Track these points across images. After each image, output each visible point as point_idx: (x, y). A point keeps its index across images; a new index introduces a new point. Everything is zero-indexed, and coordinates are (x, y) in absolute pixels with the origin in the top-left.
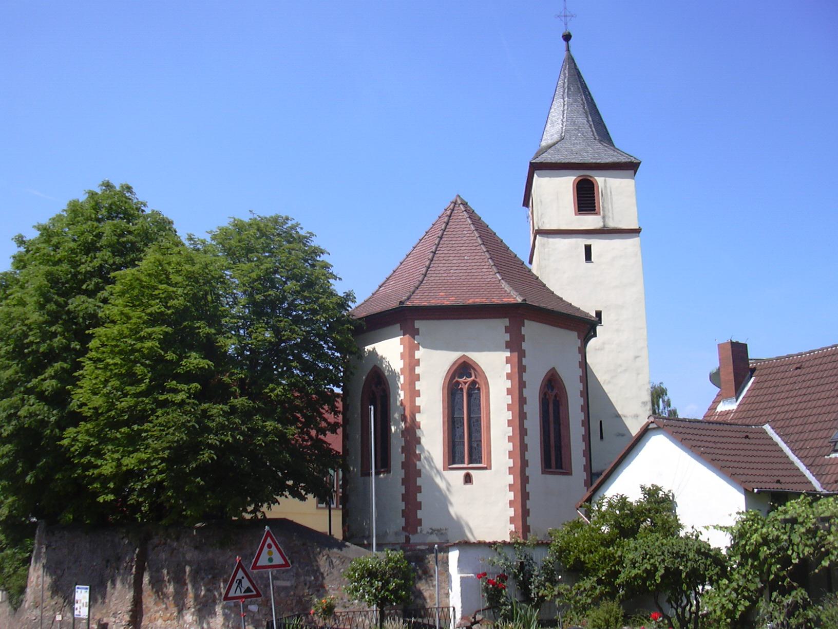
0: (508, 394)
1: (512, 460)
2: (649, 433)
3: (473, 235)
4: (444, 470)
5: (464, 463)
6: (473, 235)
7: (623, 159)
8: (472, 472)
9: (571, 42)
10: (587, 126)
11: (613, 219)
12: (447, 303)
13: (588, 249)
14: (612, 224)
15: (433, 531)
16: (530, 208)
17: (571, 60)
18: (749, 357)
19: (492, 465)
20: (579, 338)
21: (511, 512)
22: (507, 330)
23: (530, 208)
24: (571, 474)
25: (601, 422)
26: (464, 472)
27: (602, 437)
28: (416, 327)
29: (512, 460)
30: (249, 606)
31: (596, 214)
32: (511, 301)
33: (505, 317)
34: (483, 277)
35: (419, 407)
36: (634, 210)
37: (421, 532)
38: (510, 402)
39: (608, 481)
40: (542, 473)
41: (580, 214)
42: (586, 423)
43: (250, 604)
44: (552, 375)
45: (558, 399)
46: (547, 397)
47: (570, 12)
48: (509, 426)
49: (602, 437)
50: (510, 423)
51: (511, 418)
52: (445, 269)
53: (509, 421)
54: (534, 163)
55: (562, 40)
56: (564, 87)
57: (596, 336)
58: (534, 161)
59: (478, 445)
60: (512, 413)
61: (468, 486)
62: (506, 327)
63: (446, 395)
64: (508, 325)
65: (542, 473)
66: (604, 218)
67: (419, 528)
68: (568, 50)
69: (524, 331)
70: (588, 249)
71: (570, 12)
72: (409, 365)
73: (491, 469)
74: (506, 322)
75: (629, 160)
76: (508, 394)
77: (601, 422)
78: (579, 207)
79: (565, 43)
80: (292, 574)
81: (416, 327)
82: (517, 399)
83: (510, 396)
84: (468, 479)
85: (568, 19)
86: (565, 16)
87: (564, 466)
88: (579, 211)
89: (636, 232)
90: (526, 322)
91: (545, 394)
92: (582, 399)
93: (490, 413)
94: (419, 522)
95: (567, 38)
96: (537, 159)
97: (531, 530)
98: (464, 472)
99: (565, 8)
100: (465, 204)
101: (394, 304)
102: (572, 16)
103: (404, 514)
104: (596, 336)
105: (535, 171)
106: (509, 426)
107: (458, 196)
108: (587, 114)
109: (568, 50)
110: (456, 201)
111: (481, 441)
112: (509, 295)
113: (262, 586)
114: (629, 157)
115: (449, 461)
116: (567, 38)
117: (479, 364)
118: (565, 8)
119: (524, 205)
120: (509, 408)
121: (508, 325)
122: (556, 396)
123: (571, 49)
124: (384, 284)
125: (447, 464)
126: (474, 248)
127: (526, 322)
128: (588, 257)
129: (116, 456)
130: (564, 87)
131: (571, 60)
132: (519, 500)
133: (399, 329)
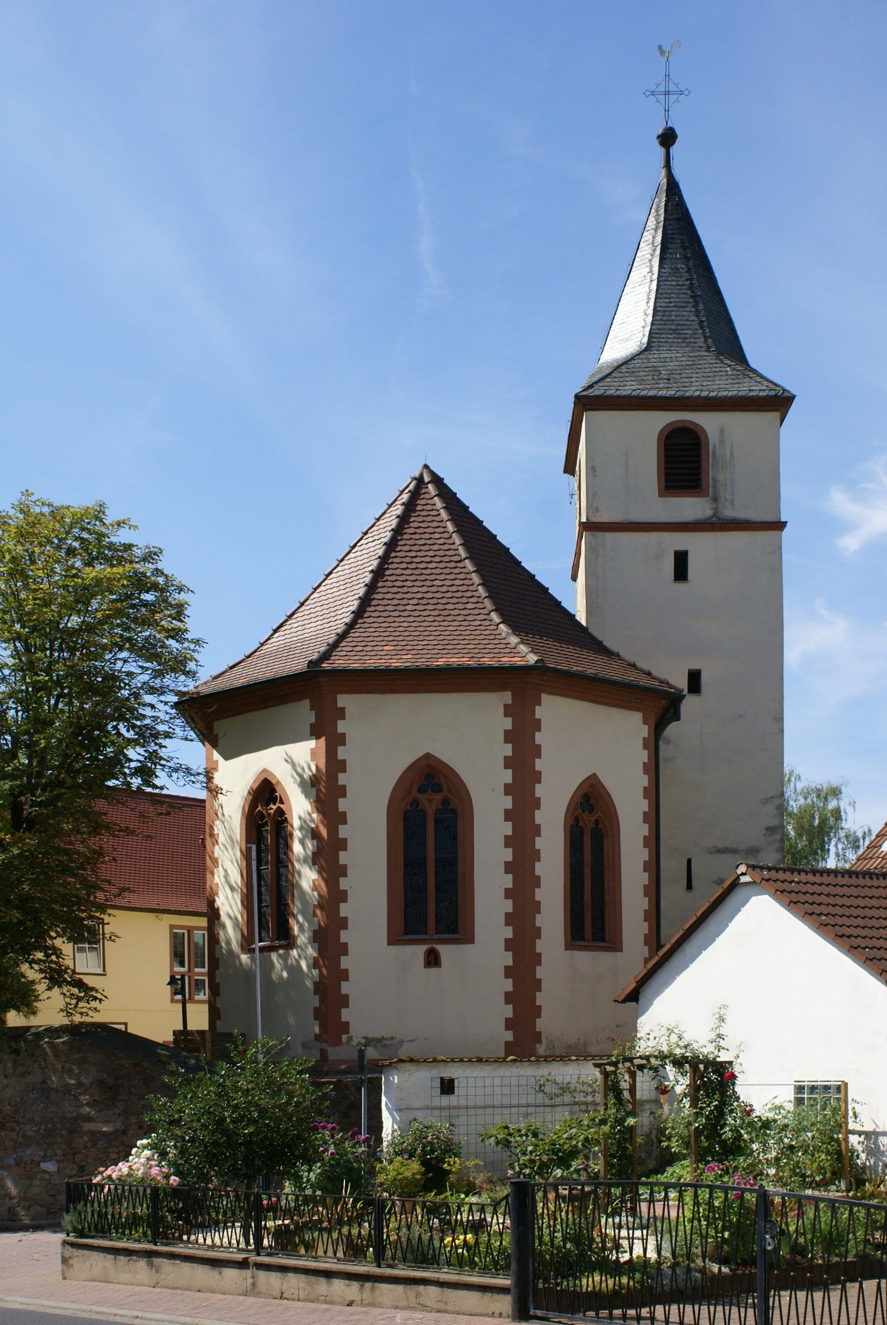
2: (738, 894)
3: (450, 541)
6: (450, 541)
7: (758, 390)
9: (674, 150)
11: (732, 503)
12: (395, 664)
13: (681, 561)
14: (729, 513)
15: (369, 1041)
16: (577, 477)
17: (673, 189)
20: (645, 723)
22: (508, 711)
23: (577, 477)
24: (621, 950)
25: (689, 861)
26: (424, 948)
27: (689, 886)
28: (340, 705)
30: (42, 1164)
32: (517, 661)
33: (504, 690)
34: (467, 618)
35: (506, 715)
37: (347, 1043)
39: (667, 963)
40: (567, 949)
42: (654, 866)
43: (44, 1161)
44: (591, 786)
45: (600, 826)
46: (581, 823)
47: (676, 85)
49: (689, 886)
52: (395, 602)
54: (587, 397)
55: (656, 143)
57: (678, 719)
58: (585, 393)
62: (506, 706)
64: (510, 702)
65: (567, 949)
67: (344, 1038)
68: (668, 165)
69: (540, 712)
70: (681, 561)
71: (676, 85)
74: (507, 697)
75: (772, 393)
77: (689, 861)
78: (667, 481)
79: (662, 150)
80: (117, 1112)
81: (340, 705)
85: (672, 98)
87: (607, 937)
90: (545, 697)
91: (577, 819)
92: (646, 827)
94: (345, 1027)
95: (668, 138)
96: (591, 391)
97: (543, 1039)
98: (424, 948)
99: (668, 76)
100: (437, 481)
103: (318, 1014)
104: (678, 719)
107: (426, 467)
109: (668, 165)
110: (421, 476)
112: (513, 651)
113: (64, 1132)
114: (773, 387)
116: (668, 138)
117: (455, 769)
118: (668, 76)
119: (566, 471)
122: (597, 822)
123: (674, 164)
124: (281, 626)
126: (452, 565)
127: (545, 697)
128: (681, 571)
130: (653, 243)
131: (673, 189)
133: (309, 708)
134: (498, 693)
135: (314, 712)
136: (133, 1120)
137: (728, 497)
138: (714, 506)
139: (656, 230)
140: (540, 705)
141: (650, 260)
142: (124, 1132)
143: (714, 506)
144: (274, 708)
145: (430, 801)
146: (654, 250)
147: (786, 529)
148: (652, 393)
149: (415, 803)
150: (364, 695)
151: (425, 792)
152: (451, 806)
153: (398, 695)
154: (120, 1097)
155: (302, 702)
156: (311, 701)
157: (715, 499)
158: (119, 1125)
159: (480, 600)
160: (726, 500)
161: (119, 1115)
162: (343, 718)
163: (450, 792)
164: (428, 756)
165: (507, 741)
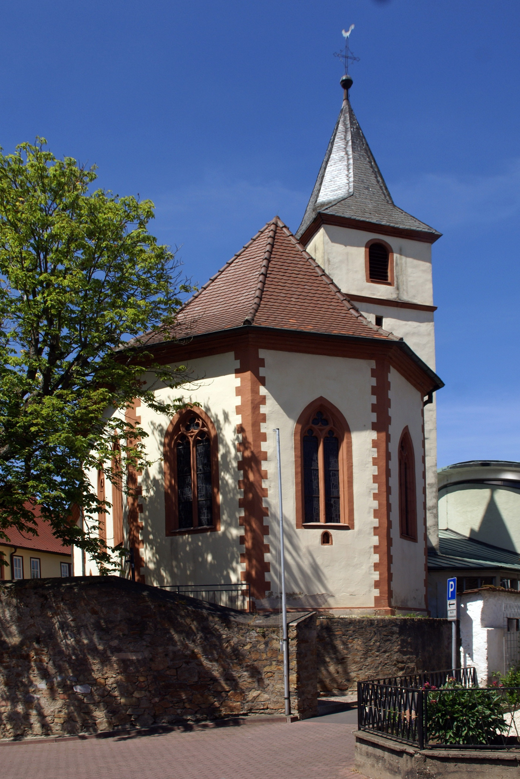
0: (373, 447)
1: (377, 520)
4: (298, 526)
5: (319, 521)
6: (308, 263)
7: (422, 228)
8: (331, 531)
9: (351, 90)
10: (378, 187)
11: (407, 293)
14: (406, 298)
18: (81, 575)
19: (355, 524)
21: (376, 576)
22: (374, 373)
26: (321, 531)
29: (377, 520)
31: (389, 284)
33: (371, 359)
36: (429, 287)
38: (376, 456)
41: (372, 282)
47: (352, 53)
48: (374, 482)
50: (375, 479)
51: (376, 473)
53: (374, 476)
56: (345, 139)
59: (335, 502)
60: (378, 468)
61: (326, 546)
62: (372, 370)
63: (299, 442)
66: (398, 289)
71: (352, 53)
72: (252, 403)
73: (353, 528)
74: (373, 364)
76: (373, 447)
78: (370, 274)
79: (343, 92)
82: (384, 454)
83: (375, 449)
84: (326, 539)
86: (347, 57)
88: (371, 278)
89: (431, 309)
93: (352, 466)
98: (321, 531)
101: (239, 323)
102: (355, 59)
105: (323, 225)
106: (374, 482)
108: (375, 174)
111: (339, 498)
115: (303, 520)
120: (375, 462)
121: (375, 367)
125: (301, 520)
129: (22, 420)
132: (386, 563)
134: (367, 361)
135: (239, 361)
136: (160, 649)
137: (405, 288)
138: (397, 292)
139: (346, 132)
140: (390, 372)
141: (345, 148)
142: (152, 660)
143: (397, 292)
144: (199, 359)
145: (321, 430)
146: (347, 143)
147: (435, 312)
148: (362, 219)
149: (311, 431)
150: (278, 351)
151: (317, 424)
152: (335, 435)
153: (301, 354)
154: (147, 632)
155: (227, 354)
156: (235, 354)
157: (398, 289)
158: (147, 654)
159: (339, 301)
160: (404, 290)
161: (147, 646)
162: (263, 366)
163: (334, 425)
164: (321, 399)
165: (373, 393)
